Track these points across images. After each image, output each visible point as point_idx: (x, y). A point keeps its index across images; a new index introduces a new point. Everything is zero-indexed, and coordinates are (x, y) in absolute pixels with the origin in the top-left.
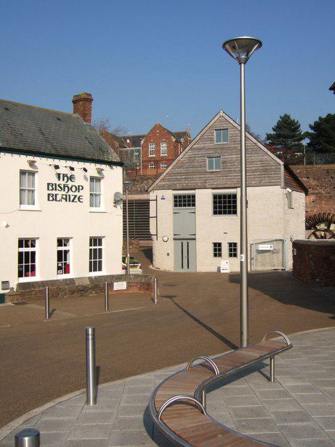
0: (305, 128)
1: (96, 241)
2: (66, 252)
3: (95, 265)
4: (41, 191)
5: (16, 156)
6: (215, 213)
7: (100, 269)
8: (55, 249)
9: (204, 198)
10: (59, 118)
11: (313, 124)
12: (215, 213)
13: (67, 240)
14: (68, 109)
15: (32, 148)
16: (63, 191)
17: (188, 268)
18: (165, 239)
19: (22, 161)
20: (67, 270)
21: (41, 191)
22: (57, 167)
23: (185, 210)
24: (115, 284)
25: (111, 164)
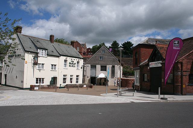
0: (120, 45)
1: (77, 76)
2: (72, 78)
3: (77, 82)
4: (68, 64)
5: (64, 57)
6: (101, 70)
7: (65, 83)
8: (63, 77)
9: (98, 67)
11: (123, 44)
12: (101, 70)
13: (66, 75)
15: (74, 56)
16: (72, 64)
17: (110, 89)
18: (88, 76)
19: (64, 58)
20: (72, 83)
21: (68, 64)
22: (72, 59)
23: (94, 70)
24: (35, 88)
25: (81, 58)
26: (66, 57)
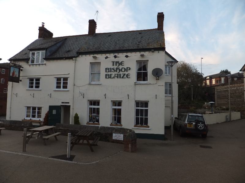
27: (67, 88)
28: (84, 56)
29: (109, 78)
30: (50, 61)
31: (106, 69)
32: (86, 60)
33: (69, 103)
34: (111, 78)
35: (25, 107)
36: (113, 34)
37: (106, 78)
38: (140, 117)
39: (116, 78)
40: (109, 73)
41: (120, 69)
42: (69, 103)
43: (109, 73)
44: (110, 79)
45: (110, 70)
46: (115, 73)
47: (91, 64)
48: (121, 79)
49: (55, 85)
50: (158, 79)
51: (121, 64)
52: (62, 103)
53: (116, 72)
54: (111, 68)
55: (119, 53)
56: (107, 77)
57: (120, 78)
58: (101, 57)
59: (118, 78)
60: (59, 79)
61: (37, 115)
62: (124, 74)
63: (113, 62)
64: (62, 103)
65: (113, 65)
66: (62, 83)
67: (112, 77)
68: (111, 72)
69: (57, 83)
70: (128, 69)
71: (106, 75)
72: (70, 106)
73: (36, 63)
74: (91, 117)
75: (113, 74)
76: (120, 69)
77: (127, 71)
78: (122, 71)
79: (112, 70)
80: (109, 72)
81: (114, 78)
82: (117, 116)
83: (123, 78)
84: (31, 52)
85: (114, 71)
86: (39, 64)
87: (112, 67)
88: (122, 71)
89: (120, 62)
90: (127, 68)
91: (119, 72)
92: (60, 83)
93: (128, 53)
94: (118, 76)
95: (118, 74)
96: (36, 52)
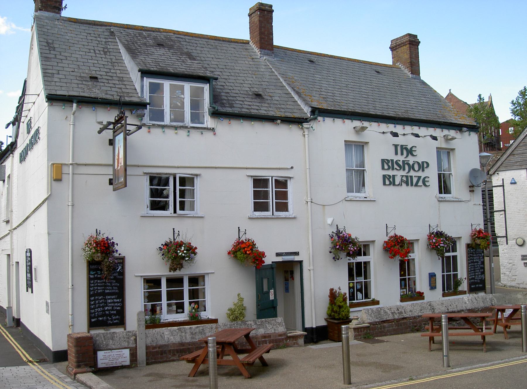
10: (377, 69)
14: (386, 58)
19: (345, 129)
26: (357, 123)
27: (286, 210)
28: (329, 120)
29: (390, 184)
30: (54, 104)
31: (383, 161)
32: (335, 133)
33: (297, 254)
34: (394, 184)
35: (140, 278)
36: (174, 37)
37: (384, 184)
38: (452, 273)
39: (404, 185)
40: (391, 173)
41: (411, 163)
42: (297, 254)
43: (391, 173)
44: (392, 187)
45: (390, 164)
46: (402, 173)
47: (348, 144)
48: (413, 187)
49: (250, 200)
50: (473, 191)
51: (410, 152)
52: (278, 255)
53: (404, 170)
54: (392, 160)
55: (422, 126)
56: (387, 182)
57: (412, 185)
58: (374, 132)
59: (407, 185)
60: (259, 183)
61: (190, 303)
62: (419, 177)
63: (396, 146)
64: (35, 269)
65: (396, 153)
66: (269, 194)
67: (397, 183)
68: (393, 169)
69: (257, 195)
70: (425, 165)
71: (384, 177)
72: (301, 262)
73: (171, 121)
74: (353, 288)
75: (399, 174)
76: (411, 163)
77: (423, 170)
78: (415, 171)
79: (396, 166)
80: (389, 169)
81: (401, 185)
82: (452, 273)
83: (416, 185)
84: (147, 81)
85: (398, 168)
86: (163, 127)
87: (395, 158)
88: (415, 171)
89: (409, 147)
90: (423, 162)
91: (402, 171)
92: (266, 195)
93: (397, 126)
94: (408, 181)
95: (407, 177)
96: (167, 84)
